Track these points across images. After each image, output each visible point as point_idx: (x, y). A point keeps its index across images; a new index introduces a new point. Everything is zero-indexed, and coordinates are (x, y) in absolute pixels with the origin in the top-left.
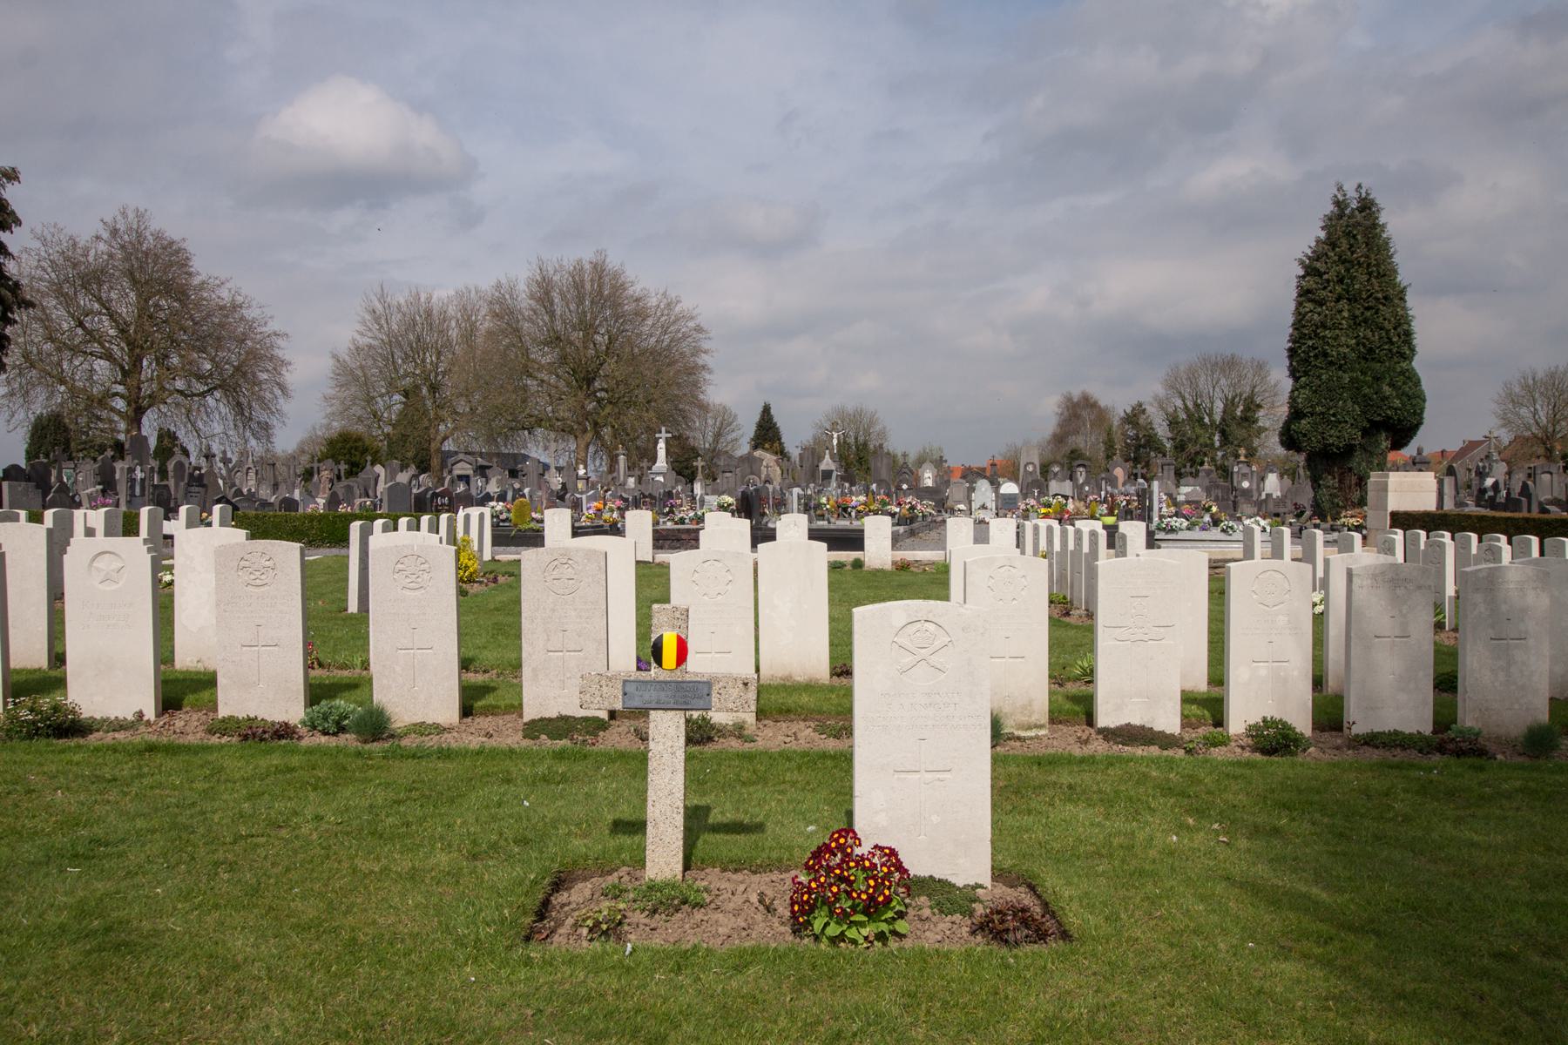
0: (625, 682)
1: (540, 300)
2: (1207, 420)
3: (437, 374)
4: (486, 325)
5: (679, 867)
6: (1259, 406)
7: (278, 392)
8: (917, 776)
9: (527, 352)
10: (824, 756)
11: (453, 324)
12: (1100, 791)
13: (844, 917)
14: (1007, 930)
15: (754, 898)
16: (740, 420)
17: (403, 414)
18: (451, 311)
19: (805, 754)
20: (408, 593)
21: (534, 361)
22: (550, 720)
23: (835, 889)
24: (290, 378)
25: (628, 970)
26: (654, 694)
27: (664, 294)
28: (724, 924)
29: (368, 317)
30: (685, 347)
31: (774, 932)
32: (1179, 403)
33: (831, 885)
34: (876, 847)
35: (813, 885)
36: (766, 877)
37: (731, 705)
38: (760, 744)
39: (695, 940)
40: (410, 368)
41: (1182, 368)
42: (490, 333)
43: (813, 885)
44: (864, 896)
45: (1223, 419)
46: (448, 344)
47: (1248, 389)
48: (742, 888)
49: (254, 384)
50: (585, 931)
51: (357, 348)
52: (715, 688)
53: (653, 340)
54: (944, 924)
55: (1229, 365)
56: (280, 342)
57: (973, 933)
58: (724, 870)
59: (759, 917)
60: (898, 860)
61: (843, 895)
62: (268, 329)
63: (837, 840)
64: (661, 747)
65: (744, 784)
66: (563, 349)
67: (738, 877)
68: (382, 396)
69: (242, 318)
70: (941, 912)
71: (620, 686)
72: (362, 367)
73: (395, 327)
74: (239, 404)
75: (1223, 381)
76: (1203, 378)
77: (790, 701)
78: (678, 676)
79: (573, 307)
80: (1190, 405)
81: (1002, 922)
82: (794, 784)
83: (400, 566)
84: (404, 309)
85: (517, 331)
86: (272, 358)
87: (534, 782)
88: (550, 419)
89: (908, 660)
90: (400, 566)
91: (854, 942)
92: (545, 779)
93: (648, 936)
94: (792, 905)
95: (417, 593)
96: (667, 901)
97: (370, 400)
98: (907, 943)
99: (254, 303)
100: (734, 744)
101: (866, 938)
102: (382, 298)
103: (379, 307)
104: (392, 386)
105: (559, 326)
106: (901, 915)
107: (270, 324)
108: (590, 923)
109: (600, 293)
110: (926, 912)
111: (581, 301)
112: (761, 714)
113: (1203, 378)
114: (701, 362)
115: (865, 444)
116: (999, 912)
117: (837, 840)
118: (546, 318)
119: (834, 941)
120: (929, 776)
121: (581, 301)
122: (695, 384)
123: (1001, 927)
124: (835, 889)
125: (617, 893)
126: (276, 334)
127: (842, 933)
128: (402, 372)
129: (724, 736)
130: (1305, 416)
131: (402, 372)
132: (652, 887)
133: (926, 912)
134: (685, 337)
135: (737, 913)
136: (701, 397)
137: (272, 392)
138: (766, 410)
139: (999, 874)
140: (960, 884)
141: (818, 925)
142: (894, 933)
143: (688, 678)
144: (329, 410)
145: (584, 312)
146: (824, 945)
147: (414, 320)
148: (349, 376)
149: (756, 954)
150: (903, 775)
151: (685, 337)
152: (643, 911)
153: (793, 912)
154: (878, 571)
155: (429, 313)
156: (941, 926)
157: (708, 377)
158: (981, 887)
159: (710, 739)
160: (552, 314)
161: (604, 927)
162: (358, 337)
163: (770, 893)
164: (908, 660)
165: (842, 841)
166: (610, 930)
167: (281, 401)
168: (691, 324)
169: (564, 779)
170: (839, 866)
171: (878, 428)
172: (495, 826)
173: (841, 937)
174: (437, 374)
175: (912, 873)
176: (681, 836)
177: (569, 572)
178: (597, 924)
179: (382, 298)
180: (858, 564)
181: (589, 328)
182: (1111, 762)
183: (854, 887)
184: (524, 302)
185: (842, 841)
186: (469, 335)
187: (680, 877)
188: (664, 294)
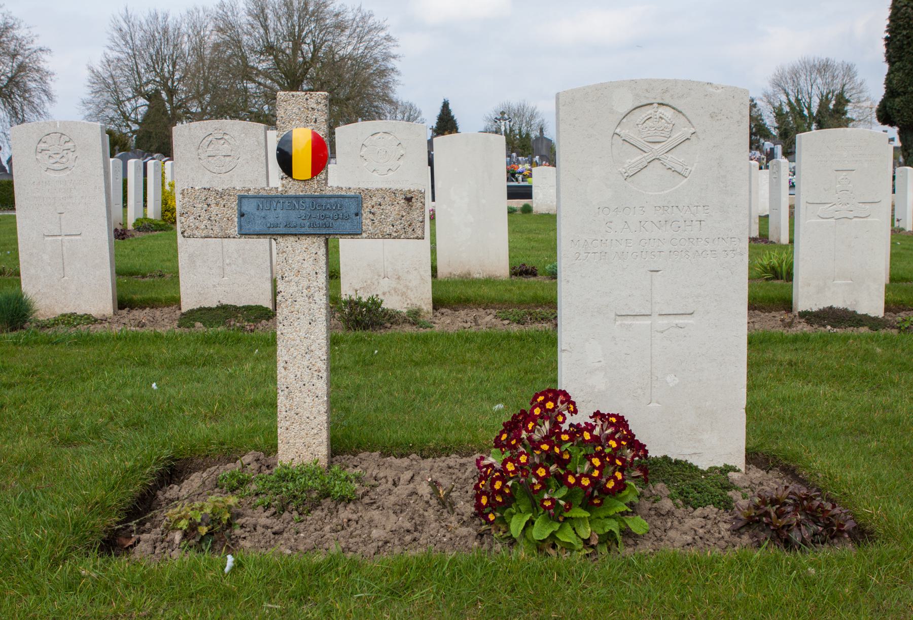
0: (241, 198)
1: (256, 17)
2: (806, 112)
3: (173, 82)
4: (213, 37)
5: (323, 451)
6: (848, 101)
7: (45, 98)
8: (647, 322)
9: (244, 58)
10: (508, 337)
11: (186, 38)
12: (827, 368)
13: (556, 514)
14: (788, 526)
15: (425, 490)
16: (423, 116)
17: (147, 116)
18: (184, 28)
19: (487, 335)
20: (52, 174)
21: (252, 67)
22: (210, 309)
23: (542, 472)
24: (54, 86)
25: (227, 595)
26: (281, 214)
27: (359, 9)
28: (382, 524)
29: (116, 34)
30: (376, 52)
31: (453, 535)
32: (784, 98)
33: (536, 467)
34: (597, 414)
35: (510, 467)
36: (441, 462)
37: (388, 229)
38: (437, 328)
39: (334, 548)
40: (151, 76)
41: (787, 70)
42: (216, 47)
43: (510, 467)
44: (586, 482)
45: (819, 112)
46: (182, 56)
47: (839, 86)
48: (407, 475)
49: (25, 91)
50: (178, 536)
51: (108, 61)
52: (367, 204)
53: (350, 48)
54: (694, 520)
55: (823, 68)
56: (44, 56)
57: (736, 531)
58: (385, 454)
59: (430, 514)
60: (629, 432)
61: (553, 482)
62: (34, 46)
63: (542, 405)
64: (293, 288)
65: (417, 364)
66: (276, 57)
67: (405, 462)
68: (129, 99)
69: (14, 38)
70: (686, 503)
71: (234, 205)
72: (112, 76)
73: (138, 43)
74: (14, 108)
75: (819, 81)
76: (803, 77)
77: (470, 292)
78: (313, 188)
79: (283, 21)
80: (793, 100)
81: (780, 514)
82: (476, 363)
83: (43, 146)
84: (145, 27)
85: (238, 43)
86: (38, 70)
87: (170, 366)
88: (266, 116)
89: (635, 159)
90: (43, 146)
91: (569, 547)
92: (186, 362)
93: (270, 543)
94: (478, 497)
95: (62, 174)
96: (303, 496)
97: (119, 103)
98: (646, 547)
99: (22, 25)
100: (408, 329)
101: (586, 542)
102: (127, 20)
103: (125, 27)
104: (138, 92)
105: (272, 38)
106: (633, 508)
107: (36, 41)
108: (184, 524)
109: (305, 8)
110: (667, 504)
111: (290, 16)
112: (437, 304)
113: (803, 77)
114: (390, 66)
115: (528, 135)
116: (774, 502)
117: (542, 405)
118: (262, 31)
119: (540, 546)
120: (665, 321)
121: (290, 16)
122: (386, 86)
123: (781, 522)
124: (542, 472)
125: (238, 485)
126: (41, 50)
127: (553, 535)
128: (144, 80)
129: (396, 323)
130: (899, 95)
131: (144, 80)
132: (285, 477)
133: (667, 504)
134: (377, 44)
135: (400, 508)
136: (391, 95)
137: (40, 98)
138: (446, 106)
139: (753, 457)
140: (704, 465)
141: (516, 526)
142: (627, 533)
143: (327, 192)
144: (87, 113)
145: (293, 25)
146: (521, 553)
147: (153, 36)
148: (106, 86)
149: (425, 568)
150: (628, 321)
151: (377, 44)
152: (267, 507)
153: (479, 506)
154: (546, 214)
155: (165, 31)
156: (689, 523)
157: (396, 78)
158: (734, 469)
159: (382, 326)
160: (266, 28)
161: (203, 530)
162: (108, 51)
163: (445, 482)
164: (635, 159)
165: (550, 405)
166: (217, 533)
167: (47, 105)
168: (382, 34)
169: (208, 362)
170: (546, 439)
171: (537, 121)
172: (107, 408)
173: (553, 541)
174: (173, 82)
175: (652, 454)
176: (323, 408)
177: (225, 148)
178: (193, 526)
179: (127, 20)
180: (527, 210)
181: (297, 42)
182: (826, 341)
183: (577, 470)
184: (243, 18)
185: (550, 405)
186: (198, 49)
187: (324, 462)
188: (359, 9)
